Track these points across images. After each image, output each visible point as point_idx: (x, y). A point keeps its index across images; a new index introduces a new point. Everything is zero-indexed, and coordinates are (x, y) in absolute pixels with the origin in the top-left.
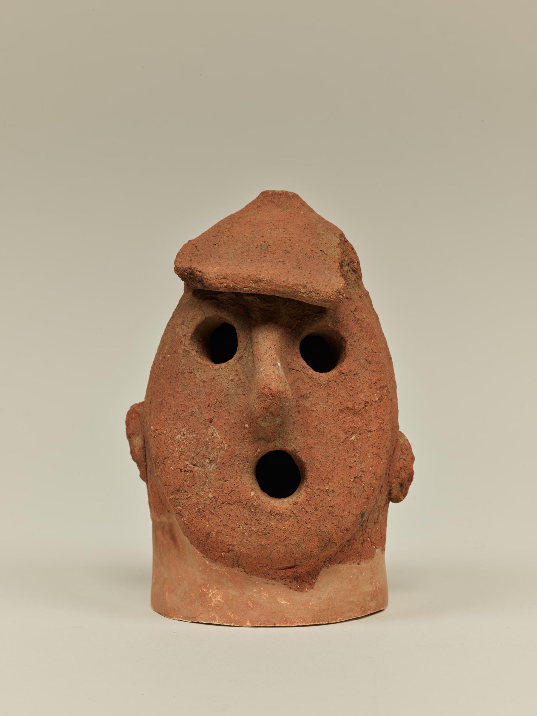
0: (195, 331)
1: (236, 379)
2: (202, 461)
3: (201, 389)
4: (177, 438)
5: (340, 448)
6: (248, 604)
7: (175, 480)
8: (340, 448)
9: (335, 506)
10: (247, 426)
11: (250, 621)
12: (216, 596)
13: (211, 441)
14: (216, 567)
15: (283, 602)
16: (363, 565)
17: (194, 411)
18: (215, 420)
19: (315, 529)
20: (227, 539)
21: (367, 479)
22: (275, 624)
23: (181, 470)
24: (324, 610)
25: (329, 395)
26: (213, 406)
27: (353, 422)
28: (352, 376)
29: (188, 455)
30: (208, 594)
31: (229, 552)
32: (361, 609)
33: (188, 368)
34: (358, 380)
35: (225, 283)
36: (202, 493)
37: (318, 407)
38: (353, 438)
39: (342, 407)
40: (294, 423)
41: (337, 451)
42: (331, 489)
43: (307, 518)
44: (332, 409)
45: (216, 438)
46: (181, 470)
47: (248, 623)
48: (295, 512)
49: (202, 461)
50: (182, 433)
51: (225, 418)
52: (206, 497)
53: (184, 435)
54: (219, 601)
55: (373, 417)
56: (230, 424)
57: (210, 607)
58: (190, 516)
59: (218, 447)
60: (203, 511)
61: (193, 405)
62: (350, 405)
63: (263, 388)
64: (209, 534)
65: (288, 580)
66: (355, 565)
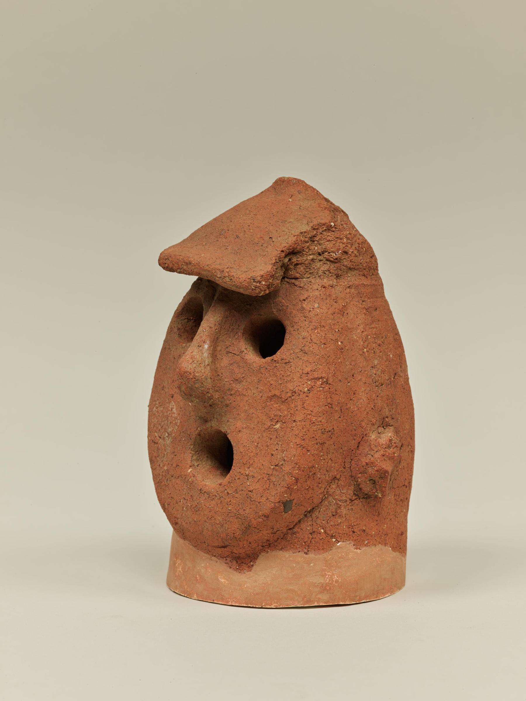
0: (183, 309)
5: (264, 435)
6: (196, 578)
8: (264, 435)
9: (254, 491)
11: (197, 594)
15: (223, 580)
16: (311, 555)
19: (235, 511)
21: (287, 468)
22: (213, 600)
24: (258, 594)
25: (259, 381)
27: (279, 410)
28: (284, 365)
32: (303, 599)
34: (289, 369)
37: (249, 391)
38: (278, 426)
39: (270, 394)
40: (227, 405)
41: (261, 437)
42: (251, 474)
43: (229, 500)
44: (261, 395)
48: (219, 493)
55: (299, 407)
62: (277, 393)
65: (229, 559)
66: (302, 554)
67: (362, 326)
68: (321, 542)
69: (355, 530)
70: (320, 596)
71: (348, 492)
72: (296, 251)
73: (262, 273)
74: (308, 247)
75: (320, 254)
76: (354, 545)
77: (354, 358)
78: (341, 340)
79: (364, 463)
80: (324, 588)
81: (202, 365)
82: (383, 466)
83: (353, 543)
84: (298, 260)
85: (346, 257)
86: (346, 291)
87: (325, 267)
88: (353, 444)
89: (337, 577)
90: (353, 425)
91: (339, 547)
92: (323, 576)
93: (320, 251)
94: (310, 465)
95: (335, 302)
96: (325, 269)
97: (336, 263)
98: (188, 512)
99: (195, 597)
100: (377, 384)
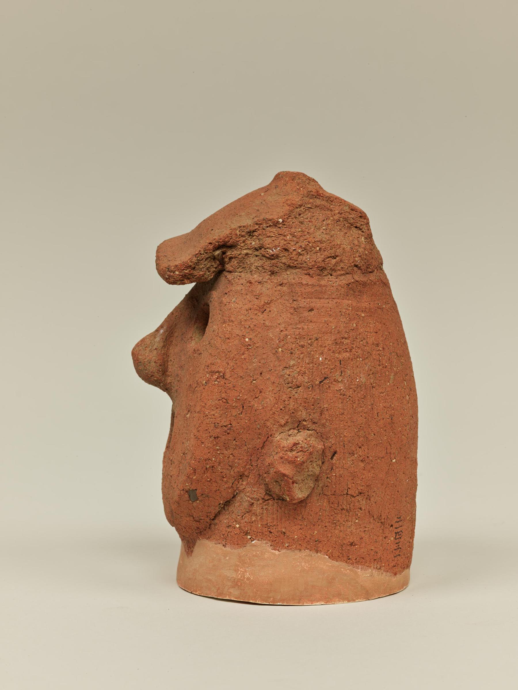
16: (228, 549)
67: (283, 325)
68: (236, 537)
69: (272, 531)
70: (232, 590)
71: (260, 492)
72: (228, 244)
73: (177, 263)
74: (244, 242)
75: (257, 250)
76: (271, 546)
77: (265, 356)
78: (251, 337)
79: (267, 464)
80: (236, 583)
81: (148, 349)
82: (280, 469)
83: (270, 544)
84: (233, 253)
85: (286, 254)
86: (275, 289)
87: (259, 263)
88: (258, 442)
89: (249, 575)
90: (257, 423)
91: (254, 545)
92: (235, 571)
93: (256, 246)
94: (206, 457)
95: (257, 298)
96: (259, 265)
97: (273, 259)
100: (290, 385)
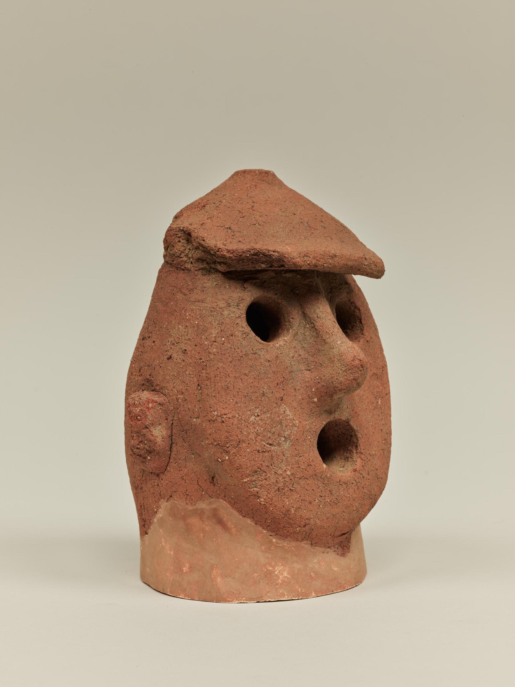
1: (296, 355)
2: (278, 439)
3: (268, 368)
4: (251, 419)
5: (374, 412)
6: (311, 576)
7: (253, 462)
10: (316, 400)
11: (315, 592)
12: (282, 572)
13: (284, 418)
14: (285, 544)
17: (265, 391)
18: (285, 398)
20: (304, 513)
23: (258, 451)
26: (281, 384)
29: (264, 436)
30: (274, 572)
31: (305, 526)
33: (251, 349)
35: (308, 260)
36: (280, 472)
45: (287, 415)
46: (258, 451)
47: (313, 594)
49: (278, 439)
50: (256, 414)
51: (293, 394)
52: (284, 475)
53: (258, 416)
54: (286, 577)
56: (298, 400)
57: (277, 584)
58: (269, 496)
59: (291, 424)
60: (283, 489)
61: (263, 385)
63: (353, 361)
64: (288, 511)
98: (326, 509)
99: (313, 595)
